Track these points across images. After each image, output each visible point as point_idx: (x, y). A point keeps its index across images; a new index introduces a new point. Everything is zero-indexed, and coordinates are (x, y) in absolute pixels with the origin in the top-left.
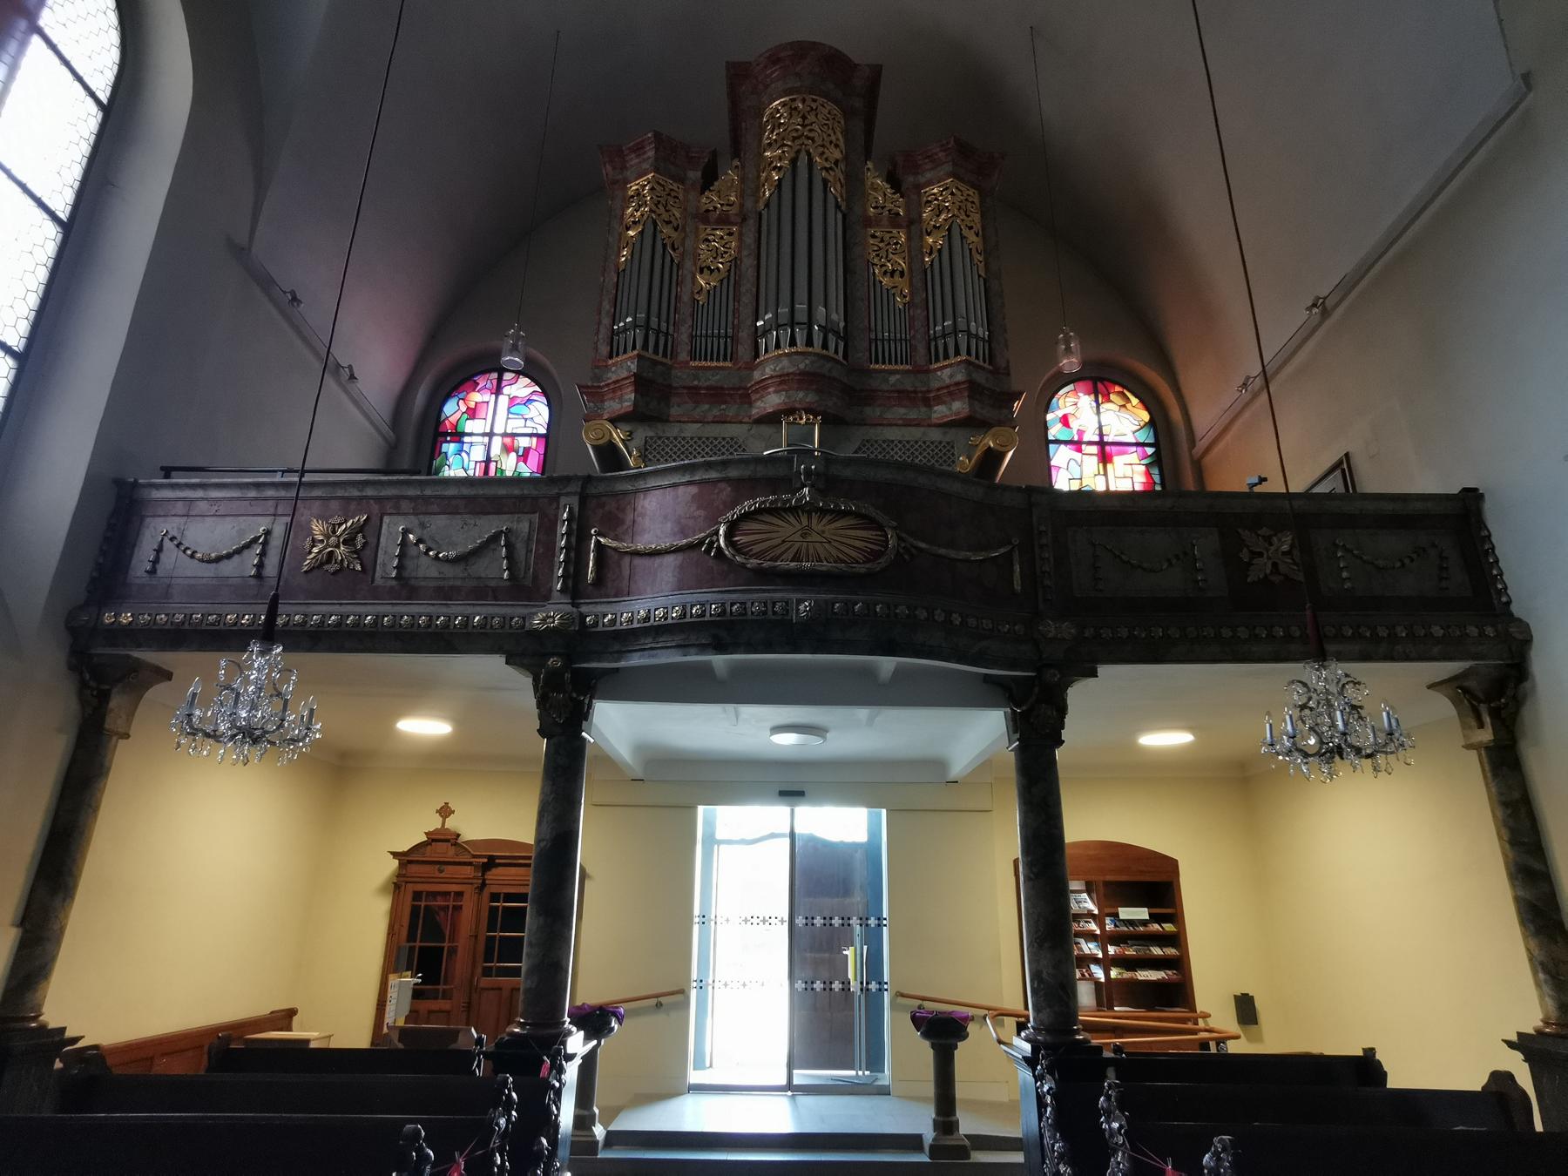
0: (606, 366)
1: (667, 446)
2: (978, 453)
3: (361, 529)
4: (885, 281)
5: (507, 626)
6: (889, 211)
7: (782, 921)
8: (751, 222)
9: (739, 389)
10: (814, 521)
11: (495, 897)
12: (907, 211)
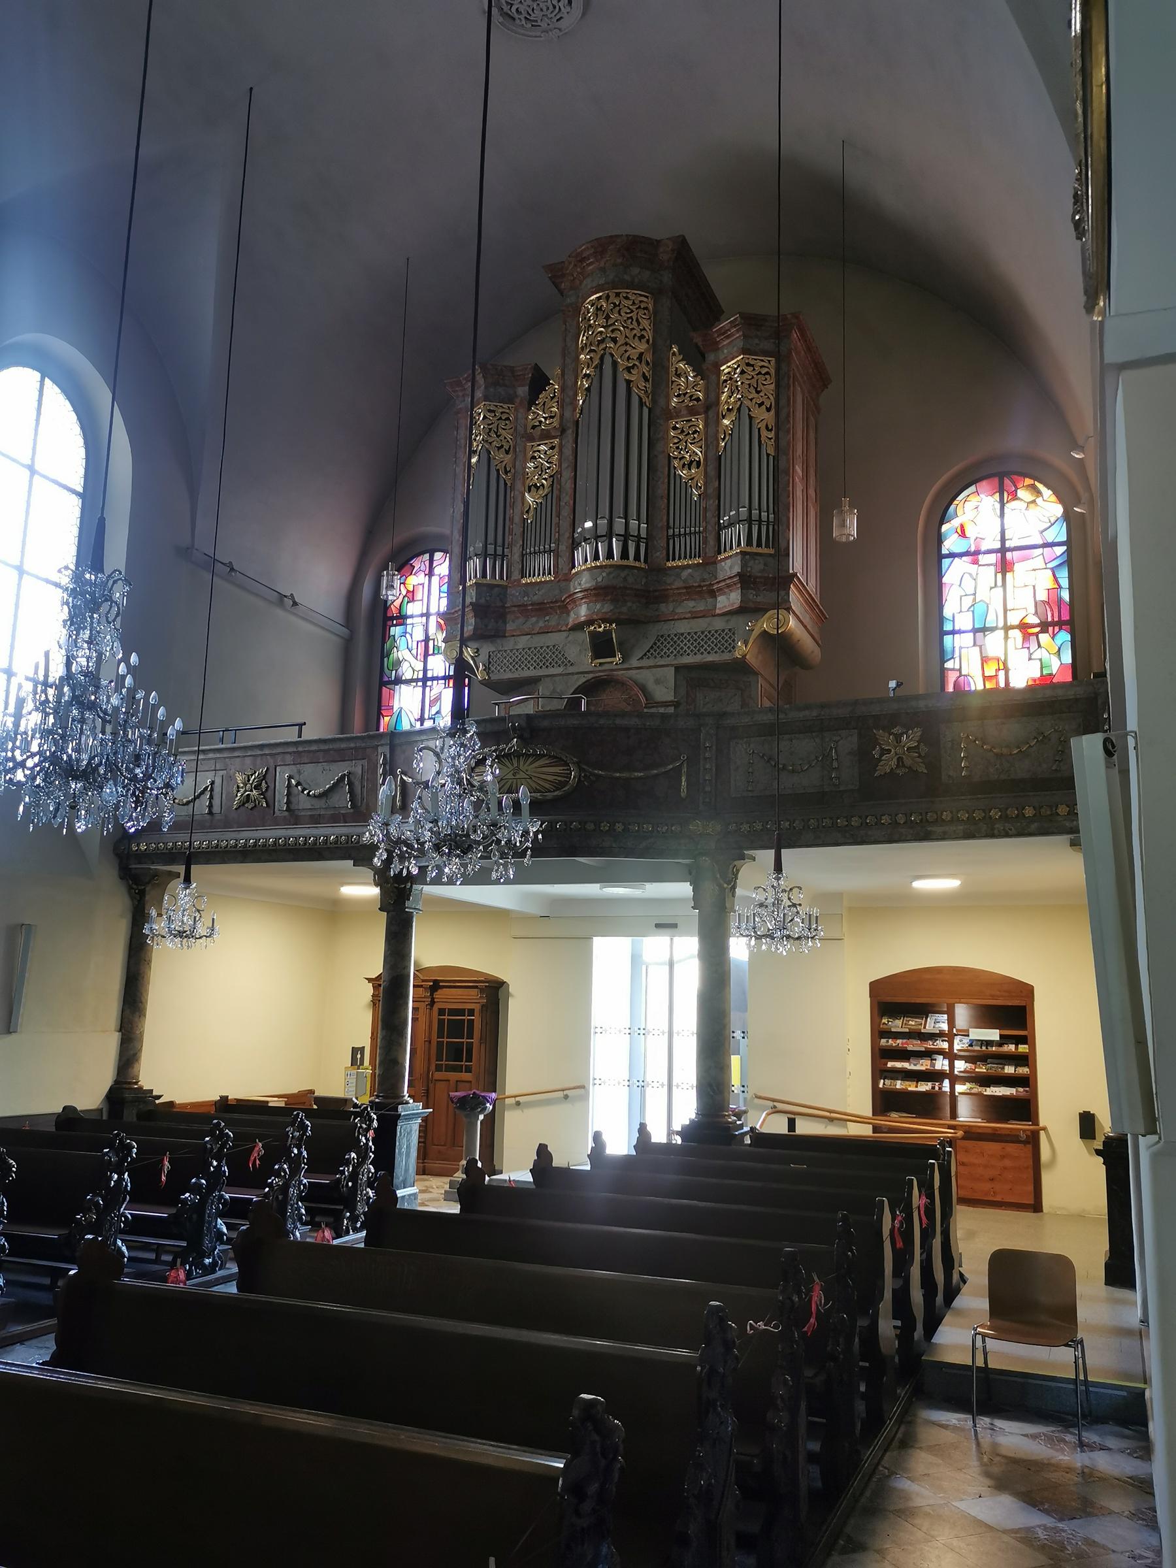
1: (505, 658)
4: (683, 473)
5: (350, 842)
7: (693, 1034)
8: (570, 432)
9: (556, 602)
10: (522, 763)
11: (441, 1012)
12: (706, 395)
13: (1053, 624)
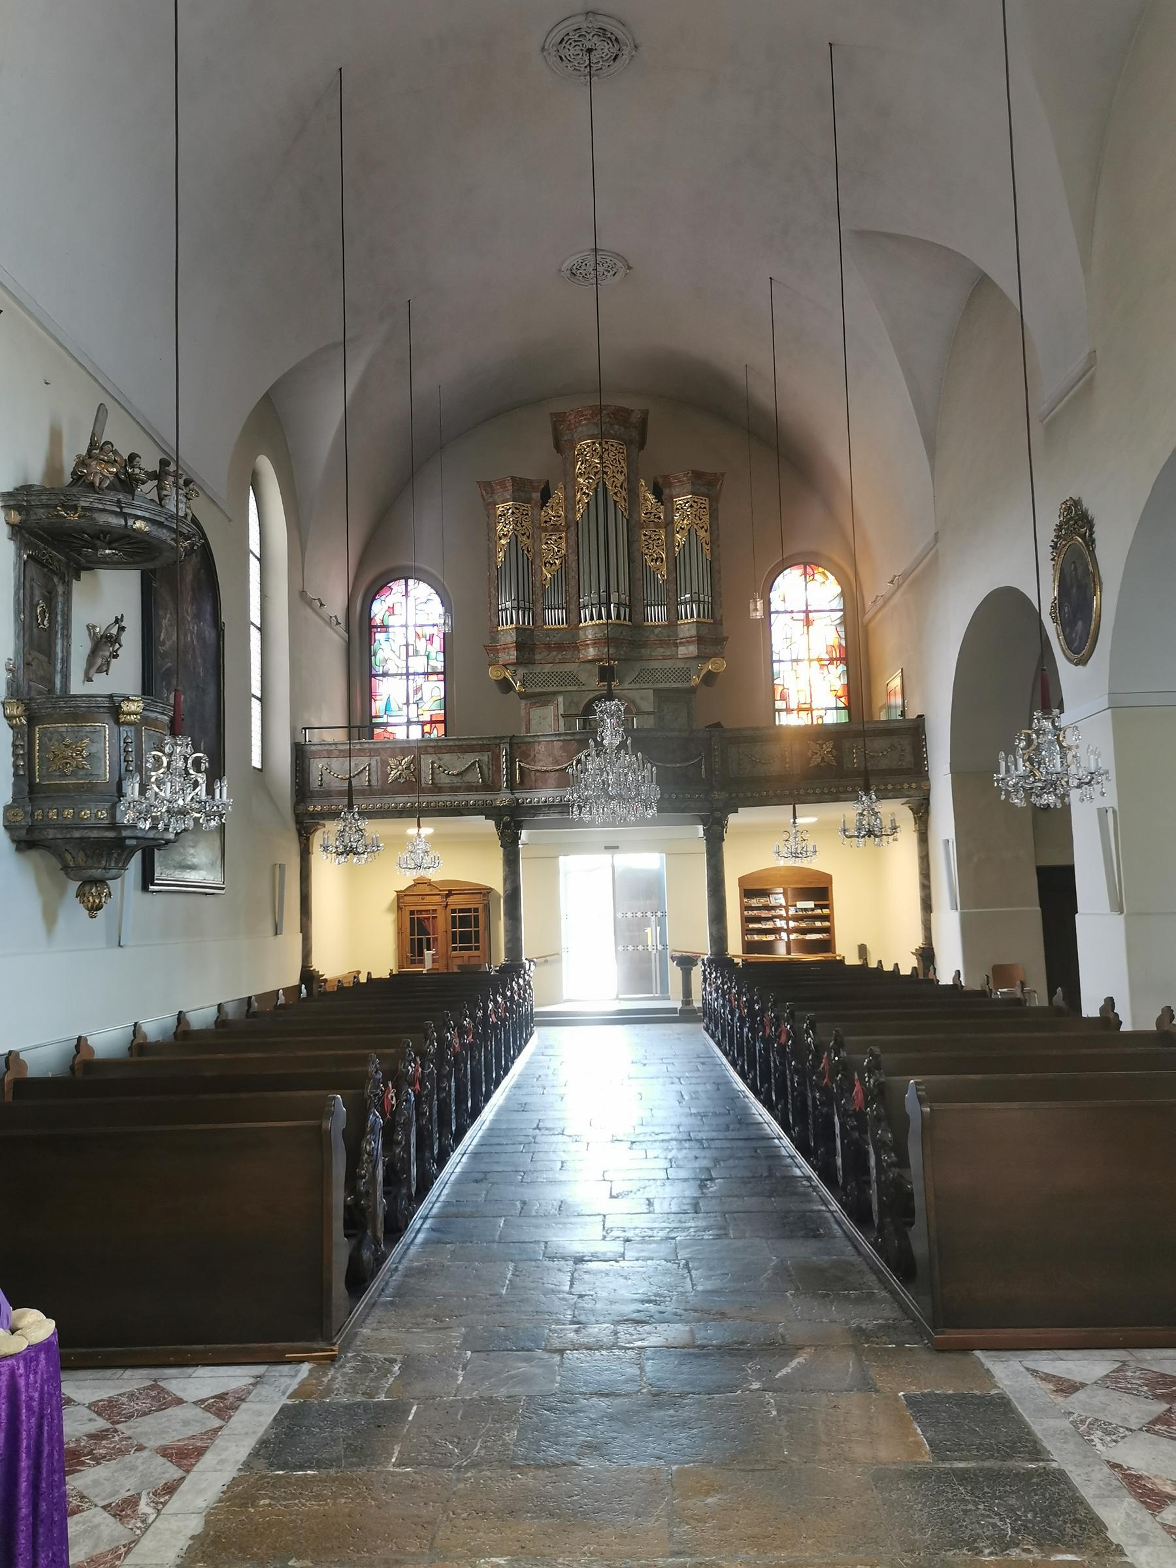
0: (498, 631)
2: (703, 673)
3: (412, 762)
6: (655, 515)
11: (453, 911)
13: (836, 659)
